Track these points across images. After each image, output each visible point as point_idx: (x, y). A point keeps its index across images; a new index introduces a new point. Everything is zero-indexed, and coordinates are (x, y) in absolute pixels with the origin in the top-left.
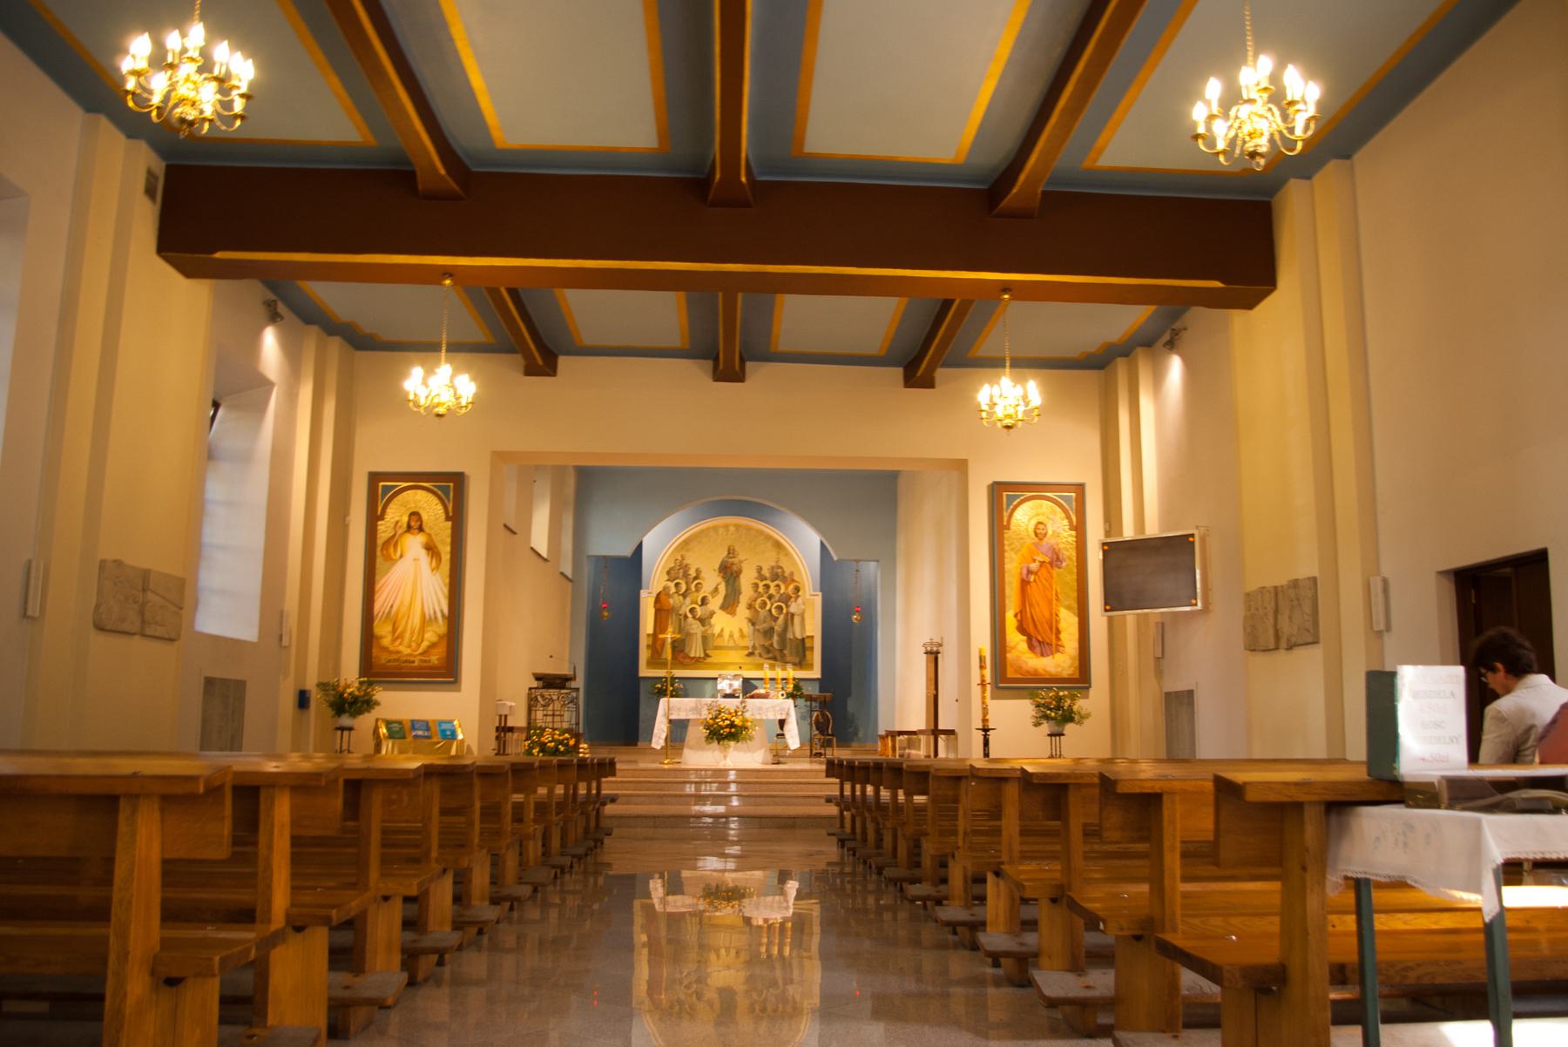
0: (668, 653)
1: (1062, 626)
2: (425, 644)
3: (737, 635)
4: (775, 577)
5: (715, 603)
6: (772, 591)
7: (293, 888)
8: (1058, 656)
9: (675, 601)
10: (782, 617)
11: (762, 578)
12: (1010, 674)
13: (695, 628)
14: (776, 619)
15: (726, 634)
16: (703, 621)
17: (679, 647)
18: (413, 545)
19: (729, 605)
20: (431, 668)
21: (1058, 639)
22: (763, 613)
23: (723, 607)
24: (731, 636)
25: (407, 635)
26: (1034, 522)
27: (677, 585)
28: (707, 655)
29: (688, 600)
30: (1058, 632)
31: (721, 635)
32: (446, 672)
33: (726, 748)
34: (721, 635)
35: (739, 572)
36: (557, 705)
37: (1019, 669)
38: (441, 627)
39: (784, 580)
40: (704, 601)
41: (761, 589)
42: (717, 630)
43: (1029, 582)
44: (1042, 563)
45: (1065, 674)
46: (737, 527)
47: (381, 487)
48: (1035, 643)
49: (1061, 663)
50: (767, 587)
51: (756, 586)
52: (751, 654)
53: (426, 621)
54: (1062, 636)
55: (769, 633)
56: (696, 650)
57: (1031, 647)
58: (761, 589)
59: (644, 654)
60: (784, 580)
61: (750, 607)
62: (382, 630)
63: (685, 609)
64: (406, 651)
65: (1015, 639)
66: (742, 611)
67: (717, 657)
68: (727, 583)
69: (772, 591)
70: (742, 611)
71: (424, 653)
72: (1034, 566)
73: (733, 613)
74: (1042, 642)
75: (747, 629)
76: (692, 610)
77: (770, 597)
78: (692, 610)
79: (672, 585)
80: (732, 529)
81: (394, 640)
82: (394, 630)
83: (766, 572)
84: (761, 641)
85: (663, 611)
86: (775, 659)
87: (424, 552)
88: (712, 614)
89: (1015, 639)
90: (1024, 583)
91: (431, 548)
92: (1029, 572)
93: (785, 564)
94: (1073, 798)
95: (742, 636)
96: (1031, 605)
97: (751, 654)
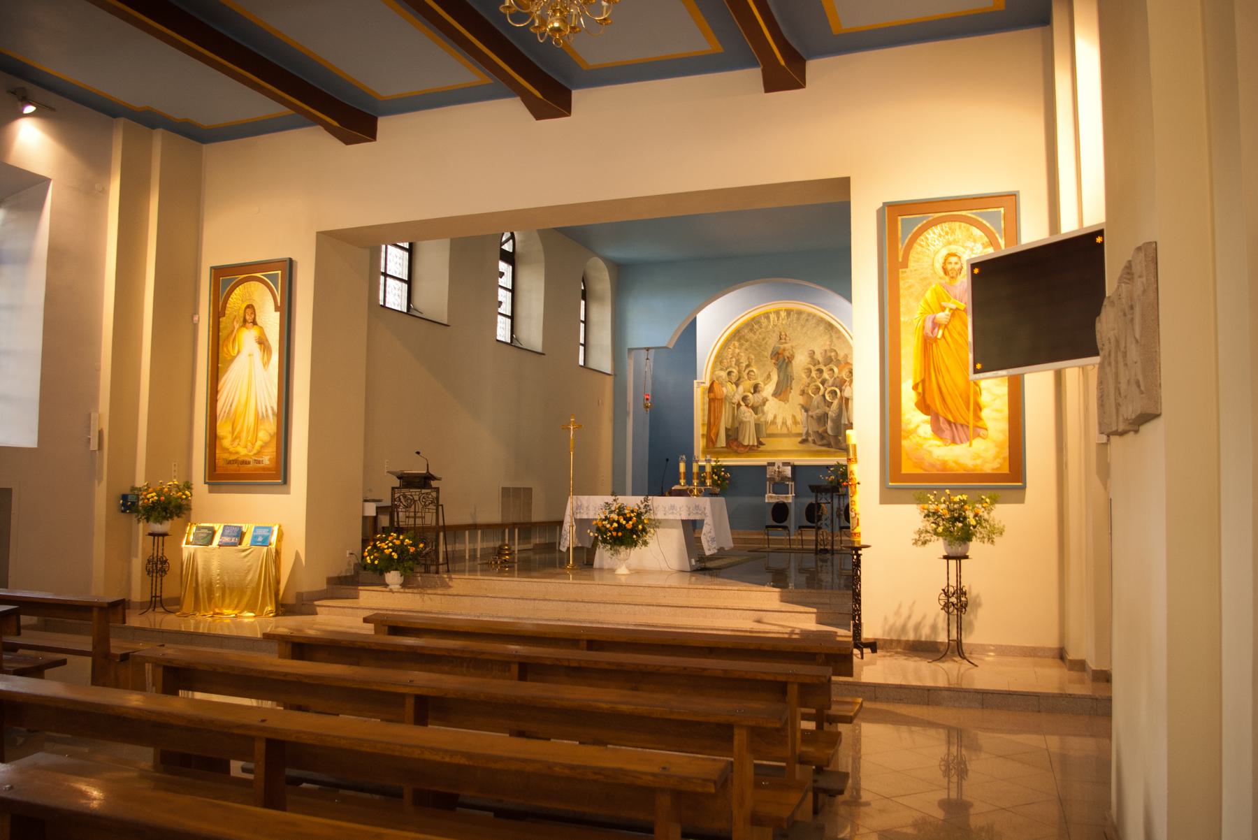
0: (722, 441)
1: (984, 399)
2: (259, 443)
3: (789, 422)
4: (828, 361)
5: (768, 390)
6: (826, 375)
7: (117, 686)
8: (978, 444)
9: (728, 389)
10: (836, 402)
11: (816, 363)
12: (906, 468)
13: (747, 415)
14: (829, 405)
15: (779, 421)
16: (755, 409)
17: (733, 437)
18: (247, 339)
19: (781, 392)
20: (264, 469)
21: (978, 418)
22: (816, 399)
23: (775, 395)
24: (784, 423)
25: (244, 434)
26: (944, 252)
27: (729, 373)
28: (760, 443)
29: (741, 388)
30: (978, 407)
31: (774, 422)
32: (279, 475)
33: (617, 552)
34: (774, 422)
35: (790, 360)
36: (419, 506)
37: (919, 462)
38: (271, 426)
39: (838, 363)
40: (756, 389)
41: (814, 374)
42: (770, 417)
43: (936, 339)
44: (954, 312)
45: (988, 468)
46: (789, 312)
47: (227, 277)
48: (945, 426)
49: (982, 452)
50: (820, 371)
51: (810, 371)
52: (804, 441)
53: (259, 419)
54: (984, 414)
55: (823, 418)
56: (749, 438)
57: (937, 431)
58: (814, 374)
59: (699, 443)
60: (838, 363)
61: (803, 393)
62: (223, 430)
63: (737, 398)
64: (243, 451)
65: (914, 419)
66: (795, 398)
67: (770, 444)
68: (779, 370)
69: (826, 375)
70: (795, 398)
71: (258, 453)
72: (942, 316)
73: (785, 400)
74: (953, 421)
75: (801, 416)
76: (744, 398)
77: (823, 383)
78: (744, 398)
79: (724, 374)
80: (783, 314)
81: (233, 440)
82: (233, 429)
83: (819, 357)
84: (814, 427)
85: (714, 400)
86: (829, 445)
87: (257, 346)
88: (765, 401)
89: (914, 419)
90: (928, 344)
91: (262, 342)
92: (936, 325)
93: (838, 346)
94: (789, 687)
95: (795, 423)
96: (938, 371)
97: (804, 441)
